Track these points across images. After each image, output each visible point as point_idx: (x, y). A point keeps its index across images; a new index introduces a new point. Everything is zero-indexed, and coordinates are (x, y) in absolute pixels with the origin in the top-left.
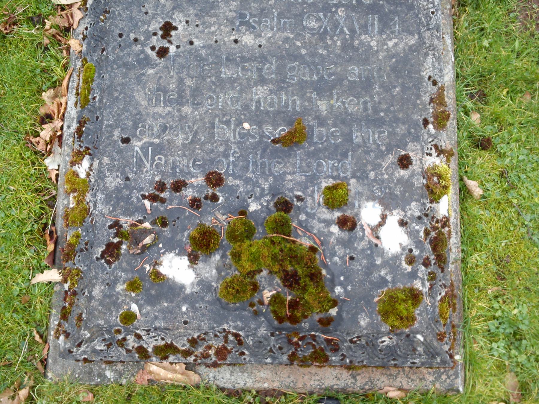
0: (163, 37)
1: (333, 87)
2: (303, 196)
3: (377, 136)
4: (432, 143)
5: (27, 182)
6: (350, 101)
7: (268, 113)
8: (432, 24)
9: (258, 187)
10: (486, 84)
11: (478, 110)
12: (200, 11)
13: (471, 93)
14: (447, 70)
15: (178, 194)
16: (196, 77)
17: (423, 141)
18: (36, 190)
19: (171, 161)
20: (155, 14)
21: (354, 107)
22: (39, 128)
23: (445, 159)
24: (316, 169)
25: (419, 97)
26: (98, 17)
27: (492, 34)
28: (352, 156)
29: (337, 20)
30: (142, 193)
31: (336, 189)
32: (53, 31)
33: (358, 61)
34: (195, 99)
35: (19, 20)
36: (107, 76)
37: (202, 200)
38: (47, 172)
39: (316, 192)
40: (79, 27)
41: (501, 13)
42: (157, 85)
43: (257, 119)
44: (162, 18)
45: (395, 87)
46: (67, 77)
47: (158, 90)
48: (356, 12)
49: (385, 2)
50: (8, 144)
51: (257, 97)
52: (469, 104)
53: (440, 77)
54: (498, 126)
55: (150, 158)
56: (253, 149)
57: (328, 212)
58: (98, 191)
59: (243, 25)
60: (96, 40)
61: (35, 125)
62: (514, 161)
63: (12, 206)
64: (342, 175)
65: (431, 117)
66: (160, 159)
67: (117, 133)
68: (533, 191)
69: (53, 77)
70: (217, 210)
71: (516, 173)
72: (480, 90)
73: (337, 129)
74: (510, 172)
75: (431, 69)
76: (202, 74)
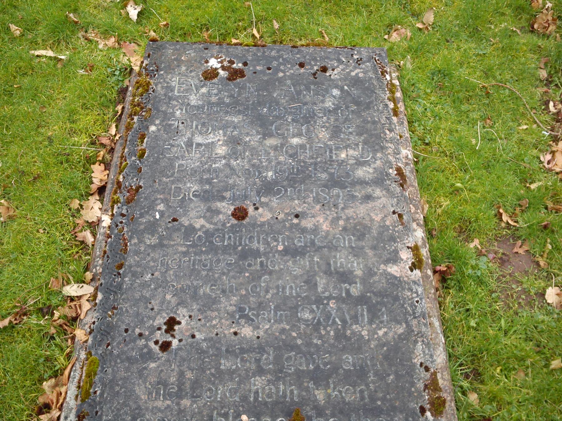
0: (167, 331)
1: (329, 376)
6: (347, 390)
7: (266, 403)
10: (479, 363)
11: (475, 390)
12: (203, 306)
13: (466, 372)
14: (439, 352)
16: (196, 370)
20: (160, 310)
25: (413, 384)
26: (106, 313)
27: (477, 314)
29: (329, 312)
32: (61, 321)
34: (194, 392)
35: (30, 311)
40: (87, 317)
41: (483, 294)
42: (158, 378)
44: (167, 313)
47: (159, 383)
49: (372, 294)
51: (256, 387)
52: (465, 384)
54: (497, 405)
60: (102, 334)
65: (428, 404)
69: (55, 366)
72: (474, 369)
75: (422, 355)
76: (202, 366)
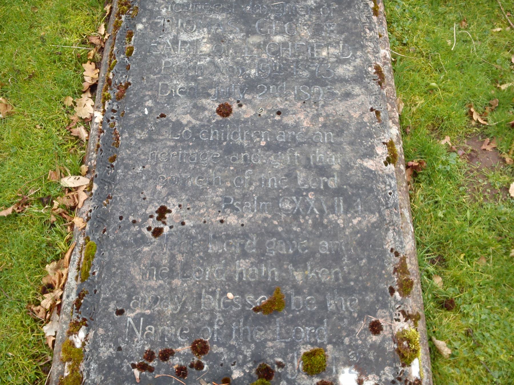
0: (158, 219)
1: (306, 260)
2: (284, 363)
3: (348, 303)
4: (400, 309)
5: (25, 349)
6: (323, 271)
7: (249, 283)
8: (390, 203)
9: (241, 354)
10: (444, 250)
11: (439, 274)
12: (191, 196)
13: (432, 258)
14: (408, 240)
15: (165, 362)
16: (186, 253)
17: (390, 308)
18: (33, 356)
19: (160, 331)
20: (152, 200)
21: (326, 277)
22: (41, 298)
23: (412, 323)
24: (295, 336)
25: (383, 267)
26: (102, 202)
27: (445, 206)
28: (327, 322)
29: (308, 202)
30: (132, 362)
31: (314, 355)
32: (60, 210)
33: (328, 237)
34: (184, 273)
35: (31, 200)
36: (106, 254)
37: (188, 368)
38: (44, 339)
39: (296, 359)
41: (451, 188)
42: (151, 260)
43: (240, 289)
44: (158, 203)
45: (362, 259)
46: (70, 251)
47: (152, 265)
48: (323, 196)
49: (348, 187)
50: (11, 312)
51: (240, 269)
52: (431, 269)
53: (401, 248)
54: (459, 288)
55: (141, 328)
56: (236, 317)
57: (307, 378)
58: (92, 361)
59: (228, 208)
60: (98, 221)
61: (37, 295)
62: (478, 321)
63: (9, 372)
64: (319, 341)
65: (396, 285)
66: (150, 329)
67: (112, 306)
68: (498, 348)
69: (56, 251)
70: (202, 378)
71: (480, 332)
72: (439, 255)
73: (313, 297)
74: (474, 330)
75: (393, 242)
76: (192, 250)
